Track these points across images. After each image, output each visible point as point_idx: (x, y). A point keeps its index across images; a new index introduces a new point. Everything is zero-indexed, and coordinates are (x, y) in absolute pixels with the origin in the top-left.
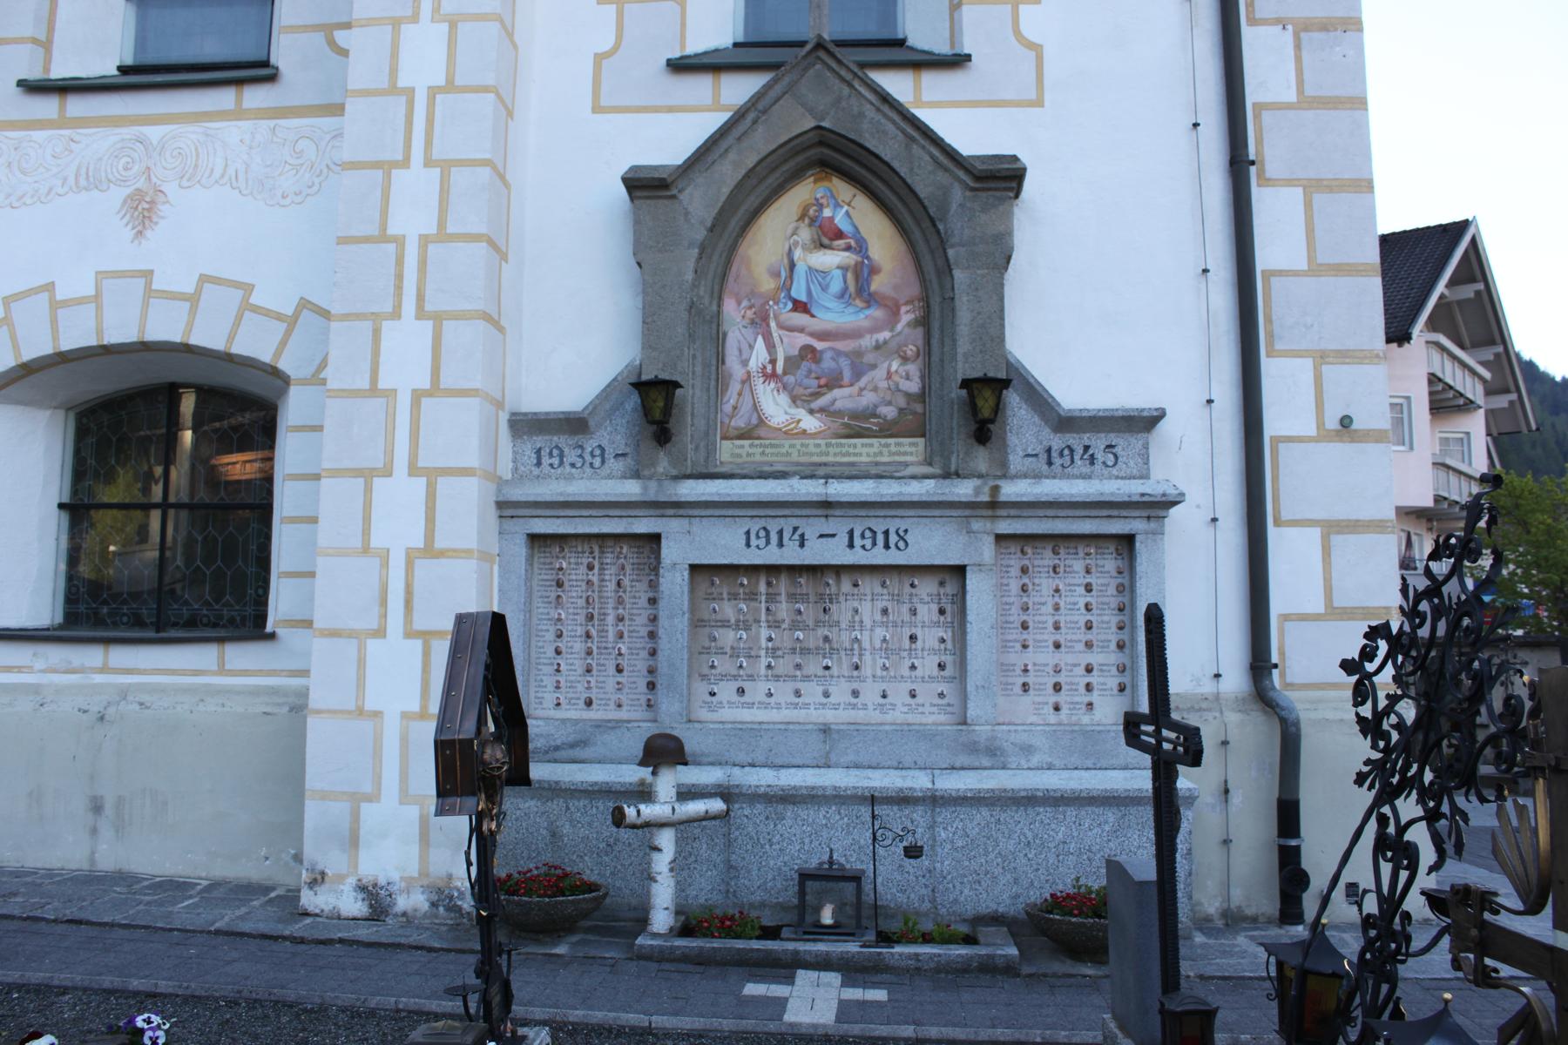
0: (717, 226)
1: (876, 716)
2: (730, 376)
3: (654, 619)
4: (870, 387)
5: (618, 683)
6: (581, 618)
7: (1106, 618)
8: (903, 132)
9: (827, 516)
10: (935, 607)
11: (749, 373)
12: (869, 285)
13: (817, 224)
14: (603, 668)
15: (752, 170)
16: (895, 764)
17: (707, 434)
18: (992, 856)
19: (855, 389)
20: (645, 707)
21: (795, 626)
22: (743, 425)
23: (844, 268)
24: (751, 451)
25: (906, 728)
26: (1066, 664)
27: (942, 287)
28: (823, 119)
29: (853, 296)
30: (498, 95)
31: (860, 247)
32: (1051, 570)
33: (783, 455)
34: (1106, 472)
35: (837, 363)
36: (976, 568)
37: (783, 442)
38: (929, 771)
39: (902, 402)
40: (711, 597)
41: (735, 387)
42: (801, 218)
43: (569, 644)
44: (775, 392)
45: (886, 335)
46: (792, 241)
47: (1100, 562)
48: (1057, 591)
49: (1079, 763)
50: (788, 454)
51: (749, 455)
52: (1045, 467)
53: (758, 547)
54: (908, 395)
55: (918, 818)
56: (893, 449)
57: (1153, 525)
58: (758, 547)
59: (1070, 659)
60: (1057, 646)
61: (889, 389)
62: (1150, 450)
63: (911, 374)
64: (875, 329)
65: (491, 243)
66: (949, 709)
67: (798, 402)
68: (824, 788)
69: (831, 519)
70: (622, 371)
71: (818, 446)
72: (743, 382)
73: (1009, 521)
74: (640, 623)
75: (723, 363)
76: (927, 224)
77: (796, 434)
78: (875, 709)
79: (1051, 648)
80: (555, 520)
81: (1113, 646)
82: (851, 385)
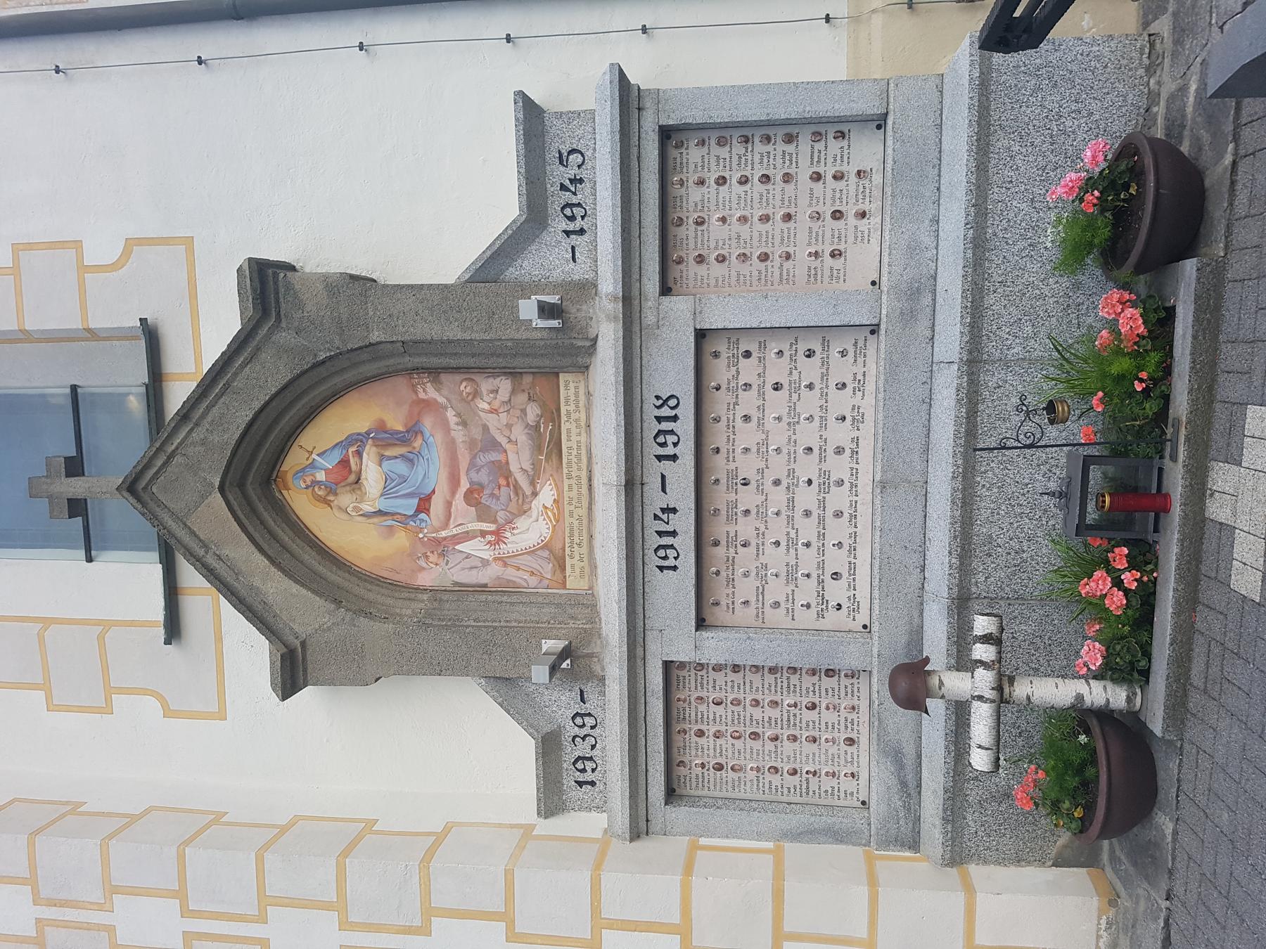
0: (336, 598)
1: (867, 430)
2: (498, 578)
3: (756, 668)
4: (507, 433)
5: (828, 708)
6: (757, 745)
7: (757, 158)
8: (219, 396)
9: (643, 484)
10: (743, 362)
11: (495, 559)
12: (398, 432)
13: (334, 487)
14: (811, 723)
15: (272, 561)
16: (925, 407)
17: (558, 605)
18: (1046, 291)
19: (508, 447)
20: (855, 681)
21: (762, 515)
22: (551, 565)
23: (382, 459)
24: (577, 557)
25: (881, 396)
26: (810, 205)
27: (392, 355)
28: (212, 485)
29: (410, 449)
30: (187, 843)
31: (357, 441)
32: (700, 228)
33: (581, 524)
34: (589, 164)
35: (482, 466)
36: (698, 319)
37: (567, 524)
38: (935, 368)
39: (523, 397)
40: (731, 607)
41: (511, 574)
42: (328, 503)
43: (785, 760)
44: (515, 532)
45: (450, 414)
46: (354, 514)
47: (691, 207)
48: (723, 220)
49: (932, 187)
50: (580, 519)
51: (581, 560)
52: (586, 237)
53: (676, 558)
54: (513, 392)
55: (995, 379)
56: (572, 408)
57: (648, 103)
58: (676, 558)
59: (804, 201)
60: (788, 217)
61: (508, 411)
62: (564, 110)
63: (491, 388)
64: (447, 429)
65: (346, 853)
66: (861, 344)
67: (526, 507)
68: (954, 490)
69: (645, 480)
70: (492, 696)
71: (570, 486)
72: (505, 565)
73: (645, 280)
74: (761, 686)
75: (485, 586)
76: (322, 371)
77: (558, 509)
78: (858, 430)
79: (791, 224)
80: (650, 774)
81: (790, 148)
82: (505, 451)
